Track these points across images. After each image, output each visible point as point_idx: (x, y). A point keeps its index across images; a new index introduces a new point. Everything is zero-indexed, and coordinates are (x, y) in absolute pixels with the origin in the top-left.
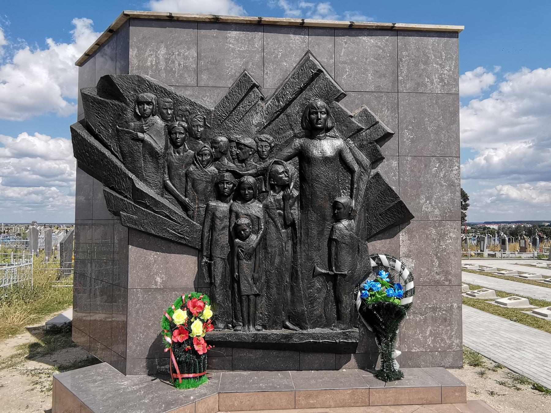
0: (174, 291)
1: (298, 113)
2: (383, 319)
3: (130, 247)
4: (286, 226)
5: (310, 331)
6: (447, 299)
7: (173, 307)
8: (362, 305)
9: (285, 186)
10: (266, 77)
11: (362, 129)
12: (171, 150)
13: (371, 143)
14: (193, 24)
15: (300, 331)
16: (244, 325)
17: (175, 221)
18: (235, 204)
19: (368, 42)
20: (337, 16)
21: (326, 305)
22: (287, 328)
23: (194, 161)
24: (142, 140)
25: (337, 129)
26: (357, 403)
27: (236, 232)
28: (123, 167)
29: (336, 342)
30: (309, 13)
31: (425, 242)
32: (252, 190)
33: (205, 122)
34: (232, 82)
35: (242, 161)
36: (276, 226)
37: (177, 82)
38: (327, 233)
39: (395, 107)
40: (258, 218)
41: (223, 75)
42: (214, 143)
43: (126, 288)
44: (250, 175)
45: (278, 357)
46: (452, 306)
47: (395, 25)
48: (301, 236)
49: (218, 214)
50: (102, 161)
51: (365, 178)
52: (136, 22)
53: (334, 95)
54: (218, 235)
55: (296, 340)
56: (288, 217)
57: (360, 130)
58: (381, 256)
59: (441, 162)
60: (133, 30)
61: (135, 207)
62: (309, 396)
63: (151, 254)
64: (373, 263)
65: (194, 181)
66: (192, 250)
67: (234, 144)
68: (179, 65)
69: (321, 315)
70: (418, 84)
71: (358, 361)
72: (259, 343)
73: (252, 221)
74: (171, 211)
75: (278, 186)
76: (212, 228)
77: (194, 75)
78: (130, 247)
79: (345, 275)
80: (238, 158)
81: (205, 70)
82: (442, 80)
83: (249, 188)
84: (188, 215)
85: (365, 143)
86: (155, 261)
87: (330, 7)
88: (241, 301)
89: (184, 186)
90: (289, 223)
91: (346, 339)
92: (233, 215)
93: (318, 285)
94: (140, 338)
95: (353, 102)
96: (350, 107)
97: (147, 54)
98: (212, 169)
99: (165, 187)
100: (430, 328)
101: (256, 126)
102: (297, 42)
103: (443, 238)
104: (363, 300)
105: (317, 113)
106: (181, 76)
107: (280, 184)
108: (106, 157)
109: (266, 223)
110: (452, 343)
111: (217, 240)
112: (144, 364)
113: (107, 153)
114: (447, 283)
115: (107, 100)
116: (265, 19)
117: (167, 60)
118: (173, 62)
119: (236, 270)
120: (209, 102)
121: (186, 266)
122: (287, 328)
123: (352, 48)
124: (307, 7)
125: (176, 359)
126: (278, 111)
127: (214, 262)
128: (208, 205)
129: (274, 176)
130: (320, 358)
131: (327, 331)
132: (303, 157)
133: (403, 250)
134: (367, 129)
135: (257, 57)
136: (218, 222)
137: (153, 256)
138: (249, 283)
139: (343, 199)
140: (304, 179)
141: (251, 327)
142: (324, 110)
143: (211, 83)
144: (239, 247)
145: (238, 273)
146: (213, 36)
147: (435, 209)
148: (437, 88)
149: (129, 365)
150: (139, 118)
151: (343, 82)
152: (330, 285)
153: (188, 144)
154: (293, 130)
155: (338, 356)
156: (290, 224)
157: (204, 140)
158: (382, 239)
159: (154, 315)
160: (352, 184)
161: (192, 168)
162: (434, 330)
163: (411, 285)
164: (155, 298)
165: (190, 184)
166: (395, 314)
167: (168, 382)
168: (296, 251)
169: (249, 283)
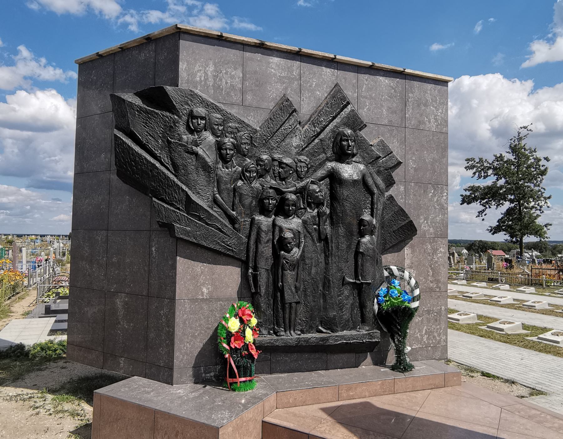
0: (220, 301)
1: (330, 138)
2: (396, 320)
3: (178, 258)
4: (320, 240)
5: (340, 333)
6: (438, 303)
7: (228, 315)
8: (379, 309)
9: (319, 204)
10: (302, 103)
11: (380, 157)
12: (220, 166)
13: (386, 170)
14: (239, 46)
15: (333, 334)
16: (285, 331)
17: (225, 234)
18: (279, 218)
19: (383, 81)
20: (226, 20)
21: (352, 310)
22: (321, 332)
23: (242, 176)
24: (196, 154)
25: (360, 155)
26: (386, 391)
27: (281, 244)
28: (176, 180)
29: (363, 342)
30: (195, 12)
31: (423, 256)
32: (295, 206)
33: (252, 140)
34: (274, 105)
35: (282, 179)
36: (313, 240)
37: (224, 99)
38: (353, 247)
39: (404, 141)
40: (299, 232)
41: (266, 97)
42: (259, 161)
43: (173, 299)
44: (291, 192)
45: (309, 359)
46: (441, 308)
47: (406, 71)
48: (332, 249)
49: (264, 228)
50: (151, 171)
51: (382, 200)
52: (186, 36)
53: (356, 123)
54: (264, 248)
55: (331, 342)
56: (323, 232)
57: (378, 157)
58: (391, 267)
59: (435, 189)
60: (184, 44)
61: (188, 219)
62: (349, 389)
63: (198, 266)
64: (386, 274)
65: (241, 195)
66: (236, 261)
67: (276, 163)
68: (227, 83)
69: (349, 319)
70: (419, 122)
71: (372, 359)
72: (301, 346)
73: (294, 234)
74: (222, 224)
75: (313, 203)
76: (258, 241)
77: (239, 95)
78: (178, 258)
79: (370, 283)
80: (280, 176)
81: (250, 91)
82: (436, 120)
83: (293, 205)
84: (234, 228)
85: (382, 169)
86: (202, 272)
87: (217, 9)
88: (283, 309)
89: (232, 200)
90: (323, 237)
91: (370, 339)
92: (277, 229)
93: (346, 293)
94: (187, 348)
95: (371, 133)
96: (370, 136)
97: (196, 69)
98: (256, 184)
99: (215, 201)
100: (425, 328)
101: (296, 148)
102: (327, 72)
103: (436, 253)
104: (379, 304)
105: (347, 140)
106: (228, 94)
107: (316, 202)
108: (157, 168)
109: (305, 236)
110: (440, 340)
111: (262, 252)
112: (190, 372)
113: (158, 165)
114: (438, 290)
115: (156, 111)
116: (304, 50)
117: (215, 77)
118: (221, 80)
119: (280, 280)
120: (255, 121)
121: (230, 276)
122: (321, 332)
123: (371, 85)
124: (193, 4)
125: (235, 363)
126: (314, 136)
127: (260, 273)
128: (253, 220)
129: (311, 194)
130: (344, 357)
131: (354, 332)
132: (334, 178)
133: (407, 262)
134: (383, 158)
135: (295, 84)
136: (263, 235)
137: (200, 267)
138: (292, 292)
139: (366, 217)
140: (334, 197)
141: (292, 332)
142: (353, 138)
143: (255, 104)
144: (284, 258)
145: (282, 282)
146: (257, 60)
147: (430, 227)
148: (433, 126)
149: (176, 375)
150: (191, 132)
151: (364, 114)
152: (356, 292)
153: (236, 160)
154: (325, 154)
155: (357, 355)
156: (323, 239)
157: (250, 158)
158: (392, 252)
159: (200, 325)
160: (372, 204)
161: (240, 183)
162: (429, 329)
163: (417, 292)
164: (202, 308)
165: (237, 198)
166: (409, 314)
167: (221, 388)
168: (329, 262)
169: (292, 292)
